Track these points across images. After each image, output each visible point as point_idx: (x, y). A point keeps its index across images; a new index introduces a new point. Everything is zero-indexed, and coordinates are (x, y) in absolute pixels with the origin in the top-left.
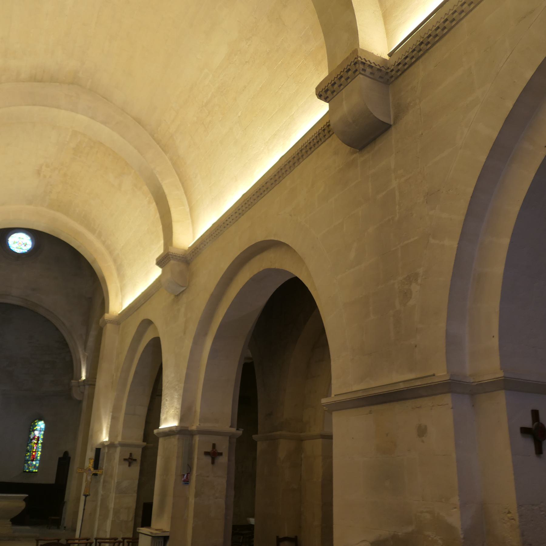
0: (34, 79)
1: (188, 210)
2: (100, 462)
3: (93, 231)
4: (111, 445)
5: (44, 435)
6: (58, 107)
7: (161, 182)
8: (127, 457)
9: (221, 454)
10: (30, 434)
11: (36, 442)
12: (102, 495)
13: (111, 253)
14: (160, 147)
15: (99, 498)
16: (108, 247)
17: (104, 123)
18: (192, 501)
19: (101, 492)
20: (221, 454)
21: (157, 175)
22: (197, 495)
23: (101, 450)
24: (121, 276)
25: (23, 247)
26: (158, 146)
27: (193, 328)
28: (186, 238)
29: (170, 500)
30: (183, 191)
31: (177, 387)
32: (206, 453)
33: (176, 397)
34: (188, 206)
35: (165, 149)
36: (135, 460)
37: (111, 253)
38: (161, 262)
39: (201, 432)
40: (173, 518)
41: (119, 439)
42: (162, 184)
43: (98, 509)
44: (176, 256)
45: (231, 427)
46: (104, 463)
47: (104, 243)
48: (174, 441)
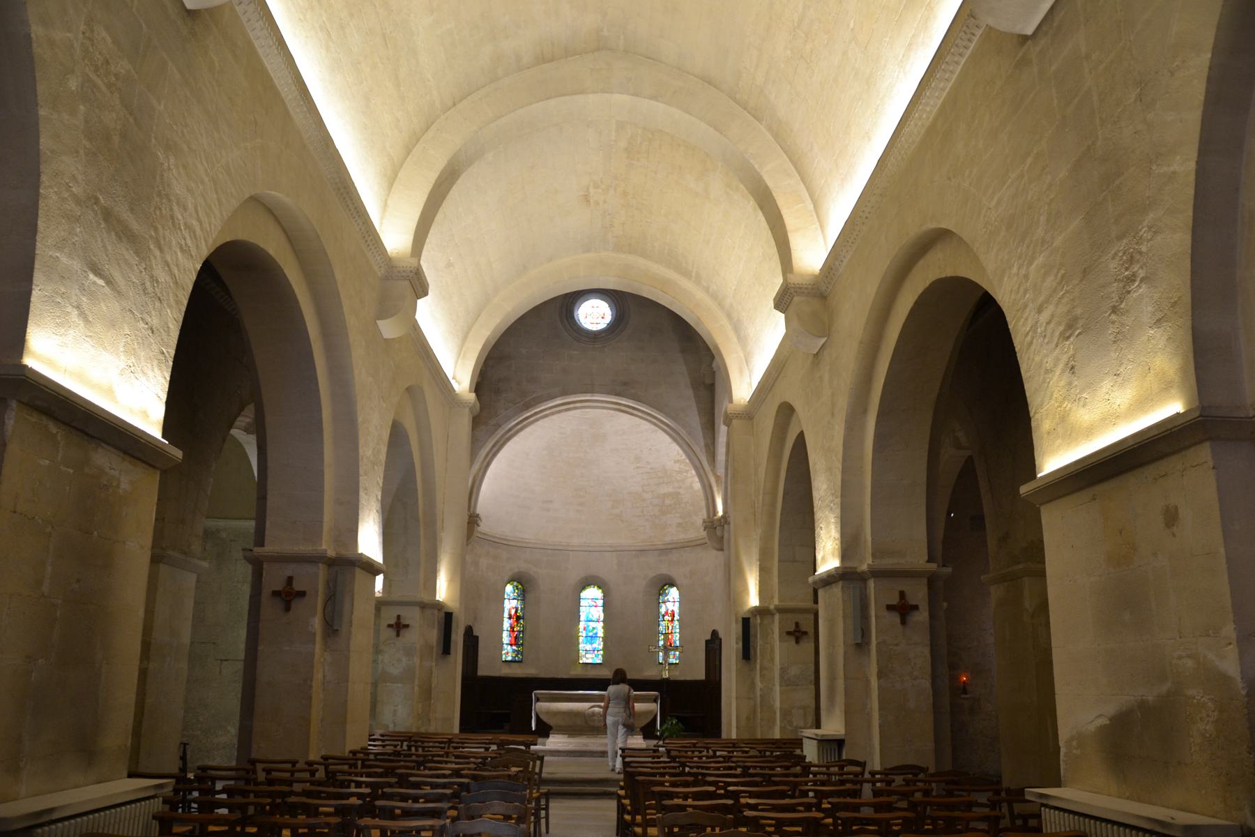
0: (542, 59)
1: (811, 207)
3: (686, 274)
4: (760, 612)
6: (582, 92)
8: (792, 628)
9: (916, 608)
10: (658, 607)
16: (714, 296)
17: (654, 97)
18: (874, 683)
19: (759, 685)
20: (916, 608)
22: (880, 675)
24: (743, 340)
25: (600, 320)
27: (843, 403)
28: (811, 255)
29: (840, 683)
32: (890, 608)
35: (756, 114)
36: (805, 633)
38: (782, 303)
39: (877, 574)
40: (849, 714)
41: (776, 602)
45: (929, 561)
46: (758, 643)
47: (707, 290)
48: (837, 590)
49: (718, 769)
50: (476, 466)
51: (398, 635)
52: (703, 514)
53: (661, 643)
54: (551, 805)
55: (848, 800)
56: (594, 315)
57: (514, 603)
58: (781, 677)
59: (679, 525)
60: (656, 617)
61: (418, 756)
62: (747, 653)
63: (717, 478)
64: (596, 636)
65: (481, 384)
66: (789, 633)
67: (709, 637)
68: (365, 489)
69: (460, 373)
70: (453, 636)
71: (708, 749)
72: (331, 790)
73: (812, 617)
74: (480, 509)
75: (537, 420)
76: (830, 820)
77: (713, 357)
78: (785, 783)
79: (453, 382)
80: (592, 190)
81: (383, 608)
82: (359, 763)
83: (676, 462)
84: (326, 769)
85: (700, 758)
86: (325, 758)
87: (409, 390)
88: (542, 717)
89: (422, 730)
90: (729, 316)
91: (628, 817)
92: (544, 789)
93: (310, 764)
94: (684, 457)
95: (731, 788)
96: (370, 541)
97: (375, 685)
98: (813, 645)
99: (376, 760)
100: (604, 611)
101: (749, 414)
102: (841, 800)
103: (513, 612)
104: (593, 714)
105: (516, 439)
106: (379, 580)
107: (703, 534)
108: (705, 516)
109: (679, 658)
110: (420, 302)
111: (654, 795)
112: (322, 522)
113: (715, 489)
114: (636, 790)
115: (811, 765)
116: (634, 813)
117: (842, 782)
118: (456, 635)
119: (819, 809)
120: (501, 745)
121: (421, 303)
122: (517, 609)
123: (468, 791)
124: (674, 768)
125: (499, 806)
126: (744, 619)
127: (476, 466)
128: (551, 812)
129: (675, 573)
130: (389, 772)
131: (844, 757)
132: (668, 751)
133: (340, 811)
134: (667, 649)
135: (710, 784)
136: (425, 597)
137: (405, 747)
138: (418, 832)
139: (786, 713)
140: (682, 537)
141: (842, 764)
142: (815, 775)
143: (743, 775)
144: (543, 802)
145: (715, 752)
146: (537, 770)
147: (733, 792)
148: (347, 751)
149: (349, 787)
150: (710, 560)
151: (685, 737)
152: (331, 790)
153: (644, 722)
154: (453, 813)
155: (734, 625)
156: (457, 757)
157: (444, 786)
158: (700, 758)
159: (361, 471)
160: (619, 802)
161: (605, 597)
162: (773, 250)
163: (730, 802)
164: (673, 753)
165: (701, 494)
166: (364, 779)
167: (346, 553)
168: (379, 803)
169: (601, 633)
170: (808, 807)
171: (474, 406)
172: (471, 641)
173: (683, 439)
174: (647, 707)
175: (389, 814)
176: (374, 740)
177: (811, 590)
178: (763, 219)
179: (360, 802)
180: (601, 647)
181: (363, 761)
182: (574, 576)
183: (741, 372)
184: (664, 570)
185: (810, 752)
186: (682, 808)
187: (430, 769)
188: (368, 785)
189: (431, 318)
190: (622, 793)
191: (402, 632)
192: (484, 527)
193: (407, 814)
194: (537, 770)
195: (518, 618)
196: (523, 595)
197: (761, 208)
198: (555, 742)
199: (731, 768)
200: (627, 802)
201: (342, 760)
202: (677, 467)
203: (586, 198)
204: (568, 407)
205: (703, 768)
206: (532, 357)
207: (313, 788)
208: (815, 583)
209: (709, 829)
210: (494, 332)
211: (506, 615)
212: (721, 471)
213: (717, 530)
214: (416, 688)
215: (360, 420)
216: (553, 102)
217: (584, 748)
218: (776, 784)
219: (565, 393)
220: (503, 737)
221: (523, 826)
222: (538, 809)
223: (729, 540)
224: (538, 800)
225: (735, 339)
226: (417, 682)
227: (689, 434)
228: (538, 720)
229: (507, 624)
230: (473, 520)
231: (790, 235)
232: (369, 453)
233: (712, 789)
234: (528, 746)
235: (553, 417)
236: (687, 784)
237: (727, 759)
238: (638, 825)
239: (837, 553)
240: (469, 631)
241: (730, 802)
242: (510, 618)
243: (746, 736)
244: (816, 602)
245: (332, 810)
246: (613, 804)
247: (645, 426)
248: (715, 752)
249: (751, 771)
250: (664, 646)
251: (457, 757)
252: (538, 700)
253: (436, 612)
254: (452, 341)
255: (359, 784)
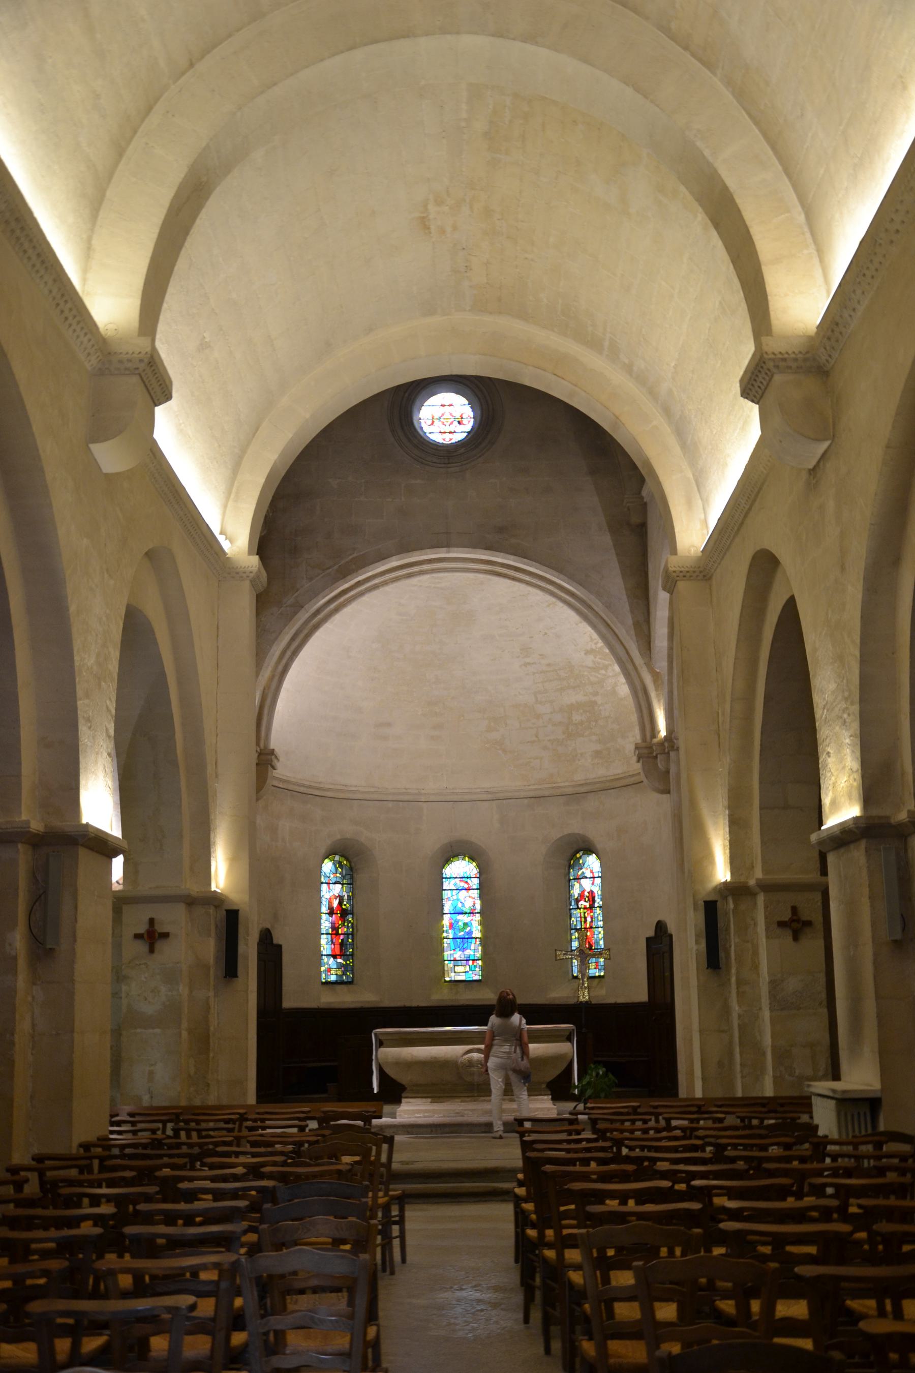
1: (802, 218)
2: (721, 936)
3: (594, 344)
4: (734, 890)
5: (603, 887)
6: (407, 34)
7: (710, 159)
8: (787, 916)
10: (569, 887)
11: (587, 905)
12: (740, 1016)
13: (653, 393)
14: (693, 55)
15: (736, 1023)
16: (641, 379)
19: (736, 1008)
21: (699, 144)
23: (718, 903)
24: (690, 449)
25: (456, 427)
26: (687, 54)
27: (859, 549)
28: (803, 303)
29: (870, 1007)
30: (780, 168)
31: (845, 716)
33: (847, 741)
34: (800, 209)
36: (809, 924)
37: (653, 393)
38: (754, 386)
41: (759, 874)
42: (716, 165)
43: (737, 1050)
44: (784, 360)
46: (733, 942)
47: (629, 369)
48: (858, 853)
49: (675, 1150)
50: (266, 673)
51: (152, 950)
52: (635, 736)
53: (575, 944)
54: (408, 1214)
55: (892, 1201)
56: (445, 418)
57: (337, 889)
58: (772, 996)
59: (597, 754)
60: (566, 903)
61: (191, 1146)
62: (714, 958)
63: (656, 676)
64: (469, 937)
65: (269, 537)
66: (781, 924)
67: (651, 933)
68: (88, 720)
69: (229, 520)
70: (241, 948)
71: (657, 1115)
72: (51, 1212)
73: (818, 897)
74: (275, 742)
75: (361, 594)
76: (863, 1235)
77: (642, 480)
78: (786, 1173)
79: (221, 539)
80: (432, 208)
81: (125, 908)
82: (96, 1163)
83: (587, 652)
84: (41, 1175)
85: (645, 1131)
86: (39, 1159)
87: (149, 555)
88: (388, 1070)
89: (197, 1102)
90: (667, 411)
91: (532, 1233)
92: (396, 1190)
93: (14, 1170)
94: (601, 644)
95: (696, 1183)
96: (99, 805)
97: (117, 1033)
98: (821, 943)
99: (123, 1156)
100: (481, 897)
101: (704, 570)
102: (881, 1202)
103: (335, 903)
104: (471, 1063)
105: (328, 626)
106: (118, 863)
107: (637, 767)
108: (638, 738)
109: (605, 968)
110: (158, 410)
111: (571, 1196)
112: (19, 776)
113: (653, 694)
114: (544, 1187)
115: (826, 1141)
116: (541, 1225)
117: (881, 1171)
118: (246, 945)
119: (846, 1217)
120: (324, 1120)
121: (161, 413)
122: (341, 898)
123: (274, 1201)
124: (603, 1149)
125: (323, 1226)
126: (706, 903)
127: (266, 673)
128: (408, 1226)
129: (594, 832)
130: (145, 1176)
131: (882, 1127)
132: (594, 1122)
133: (66, 1247)
134: (586, 953)
135: (664, 1175)
136: (192, 887)
137: (169, 1132)
138: (195, 1274)
139: (782, 1056)
140: (602, 772)
141: (880, 1139)
142: (834, 1158)
143: (719, 1157)
144: (395, 1212)
145: (668, 1120)
146: (384, 1158)
147: (701, 1188)
148: (75, 1144)
149: (79, 1205)
150: (649, 809)
151: (620, 1097)
152: (51, 1212)
153: (553, 1073)
154: (252, 1237)
155: (691, 914)
156: (254, 1144)
157: (235, 1195)
158: (645, 1131)
159: (80, 693)
160: (517, 1207)
161: (483, 874)
162: (738, 297)
163: (696, 1206)
164: (601, 1125)
165: (630, 703)
166: (104, 1191)
167: (57, 823)
168: (130, 1230)
169: (477, 934)
170: (826, 1215)
171: (258, 576)
172: (271, 954)
173: (597, 614)
174: (554, 1048)
175: (148, 1248)
176: (118, 1124)
177: (816, 854)
178: (720, 244)
179: (98, 1230)
180: (479, 955)
181: (102, 1159)
182: (431, 842)
183: (689, 503)
184: (575, 826)
185: (825, 1119)
186: (620, 1218)
187: (212, 1167)
188: (109, 1198)
189: (173, 432)
190: (521, 1191)
191: (159, 945)
192: (283, 770)
193: (176, 1245)
194: (384, 1158)
195: (344, 913)
196: (350, 874)
197: (717, 226)
198: (411, 1111)
199: (695, 1148)
200: (529, 1206)
201: (67, 1160)
202: (589, 661)
203: (424, 223)
204: (409, 571)
205: (650, 1148)
206: (346, 492)
207: (21, 1212)
208: (821, 842)
209: (664, 1251)
210: (283, 454)
211: (324, 909)
212: (661, 665)
213: (658, 761)
214: (185, 1034)
215: (73, 609)
216: (358, 55)
217: (459, 1119)
218: (771, 1174)
219: (404, 549)
220: (329, 1107)
221: (364, 1257)
222: (388, 1223)
223: (678, 775)
224: (387, 1208)
225: (677, 450)
226: (185, 1025)
227: (608, 606)
228: (382, 1074)
229: (326, 923)
230: (265, 759)
231: (763, 267)
232: (91, 661)
233: (666, 1184)
234: (367, 1119)
235: (388, 588)
236: (625, 1177)
237: (688, 1133)
238: (550, 1246)
239: (857, 793)
240: (266, 937)
241: (696, 1206)
242: (331, 912)
243: (718, 1093)
244: (824, 872)
245: (52, 1245)
246: (508, 1209)
247: (536, 596)
248: (668, 1120)
249: (730, 1152)
250: (581, 950)
251: (254, 1144)
252: (381, 1044)
253: (212, 910)
254: (212, 471)
255: (95, 1201)
